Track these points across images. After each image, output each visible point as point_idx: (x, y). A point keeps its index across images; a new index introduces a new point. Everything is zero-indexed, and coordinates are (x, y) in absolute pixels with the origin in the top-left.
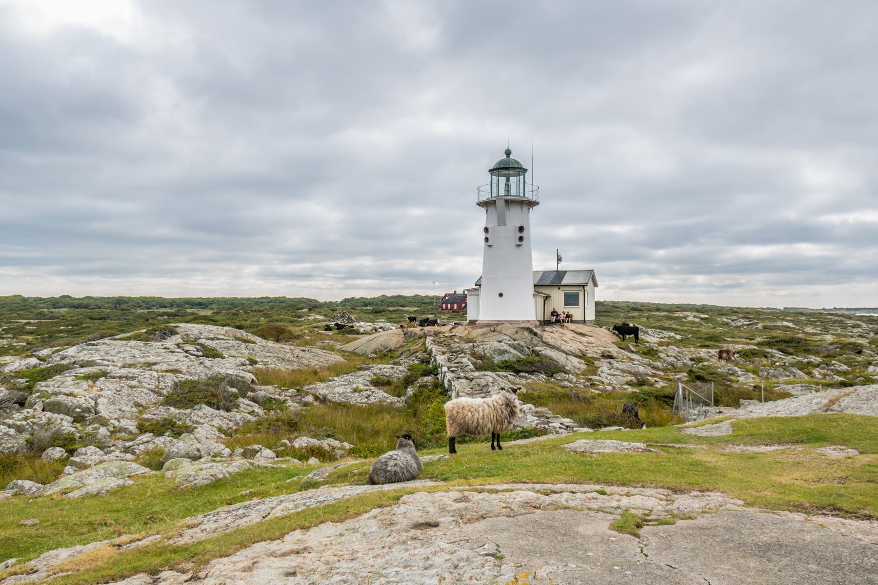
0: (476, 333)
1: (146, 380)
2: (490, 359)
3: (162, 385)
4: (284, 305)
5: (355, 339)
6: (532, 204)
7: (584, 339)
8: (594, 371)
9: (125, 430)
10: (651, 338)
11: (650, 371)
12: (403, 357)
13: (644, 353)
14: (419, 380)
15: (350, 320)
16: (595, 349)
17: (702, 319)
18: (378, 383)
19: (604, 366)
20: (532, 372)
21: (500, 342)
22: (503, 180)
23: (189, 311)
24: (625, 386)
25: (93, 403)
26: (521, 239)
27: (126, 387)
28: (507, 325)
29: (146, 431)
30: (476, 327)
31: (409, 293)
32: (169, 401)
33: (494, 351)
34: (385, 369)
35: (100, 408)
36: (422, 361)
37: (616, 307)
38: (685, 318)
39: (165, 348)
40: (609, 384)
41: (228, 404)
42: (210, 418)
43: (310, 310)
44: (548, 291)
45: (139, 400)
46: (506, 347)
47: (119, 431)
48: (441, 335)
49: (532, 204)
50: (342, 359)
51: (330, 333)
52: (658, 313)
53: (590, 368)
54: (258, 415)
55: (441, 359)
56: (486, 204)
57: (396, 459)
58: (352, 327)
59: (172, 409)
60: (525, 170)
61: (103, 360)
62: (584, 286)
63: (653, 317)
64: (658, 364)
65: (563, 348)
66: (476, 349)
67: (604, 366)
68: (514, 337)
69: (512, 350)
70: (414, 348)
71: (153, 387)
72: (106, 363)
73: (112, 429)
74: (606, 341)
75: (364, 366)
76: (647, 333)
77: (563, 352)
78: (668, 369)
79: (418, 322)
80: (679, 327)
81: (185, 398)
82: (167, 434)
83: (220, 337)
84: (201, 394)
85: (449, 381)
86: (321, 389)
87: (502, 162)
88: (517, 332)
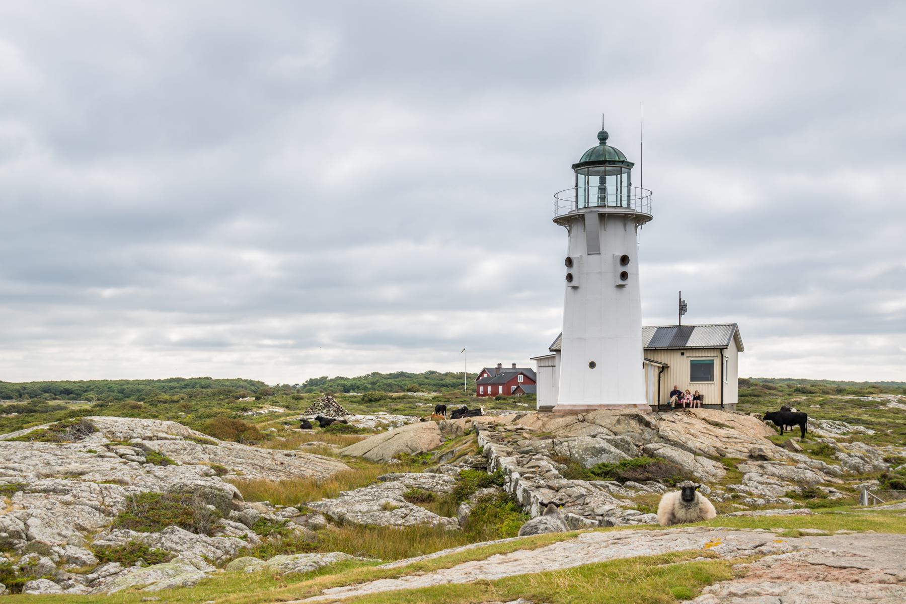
1: (84, 494)
2: (580, 463)
3: (108, 501)
4: (209, 391)
5: (358, 440)
6: (641, 219)
7: (722, 432)
8: (739, 478)
9: (75, 560)
10: (826, 432)
11: (822, 477)
12: (442, 463)
13: (814, 453)
14: (477, 493)
15: (339, 411)
16: (739, 446)
18: (416, 497)
19: (752, 470)
20: (644, 481)
21: (594, 436)
23: (52, 403)
24: (784, 499)
25: (22, 525)
26: (624, 276)
27: (58, 504)
28: (604, 411)
29: (109, 560)
30: (554, 416)
32: (124, 522)
33: (586, 450)
34: (423, 479)
35: (33, 531)
36: (476, 467)
37: (770, 388)
38: (883, 403)
39: (90, 451)
40: (761, 496)
41: (209, 526)
43: (257, 399)
44: (665, 358)
47: (68, 562)
48: (501, 429)
49: (641, 219)
52: (839, 397)
53: (732, 474)
54: (252, 541)
55: (506, 462)
56: (567, 221)
58: (345, 422)
59: (133, 533)
60: (630, 165)
61: (6, 468)
62: (721, 349)
63: (831, 402)
64: (836, 467)
65: (690, 444)
66: (557, 448)
67: (752, 470)
68: (615, 429)
69: (613, 449)
70: (459, 448)
71: (97, 503)
72: (11, 472)
73: (58, 559)
74: (755, 435)
75: (387, 475)
76: (819, 426)
77: (690, 450)
78: (850, 475)
79: (449, 414)
81: (147, 518)
82: (139, 563)
83: (161, 435)
84: (168, 512)
85: (525, 491)
86: (336, 507)
87: (593, 151)
88: (619, 422)
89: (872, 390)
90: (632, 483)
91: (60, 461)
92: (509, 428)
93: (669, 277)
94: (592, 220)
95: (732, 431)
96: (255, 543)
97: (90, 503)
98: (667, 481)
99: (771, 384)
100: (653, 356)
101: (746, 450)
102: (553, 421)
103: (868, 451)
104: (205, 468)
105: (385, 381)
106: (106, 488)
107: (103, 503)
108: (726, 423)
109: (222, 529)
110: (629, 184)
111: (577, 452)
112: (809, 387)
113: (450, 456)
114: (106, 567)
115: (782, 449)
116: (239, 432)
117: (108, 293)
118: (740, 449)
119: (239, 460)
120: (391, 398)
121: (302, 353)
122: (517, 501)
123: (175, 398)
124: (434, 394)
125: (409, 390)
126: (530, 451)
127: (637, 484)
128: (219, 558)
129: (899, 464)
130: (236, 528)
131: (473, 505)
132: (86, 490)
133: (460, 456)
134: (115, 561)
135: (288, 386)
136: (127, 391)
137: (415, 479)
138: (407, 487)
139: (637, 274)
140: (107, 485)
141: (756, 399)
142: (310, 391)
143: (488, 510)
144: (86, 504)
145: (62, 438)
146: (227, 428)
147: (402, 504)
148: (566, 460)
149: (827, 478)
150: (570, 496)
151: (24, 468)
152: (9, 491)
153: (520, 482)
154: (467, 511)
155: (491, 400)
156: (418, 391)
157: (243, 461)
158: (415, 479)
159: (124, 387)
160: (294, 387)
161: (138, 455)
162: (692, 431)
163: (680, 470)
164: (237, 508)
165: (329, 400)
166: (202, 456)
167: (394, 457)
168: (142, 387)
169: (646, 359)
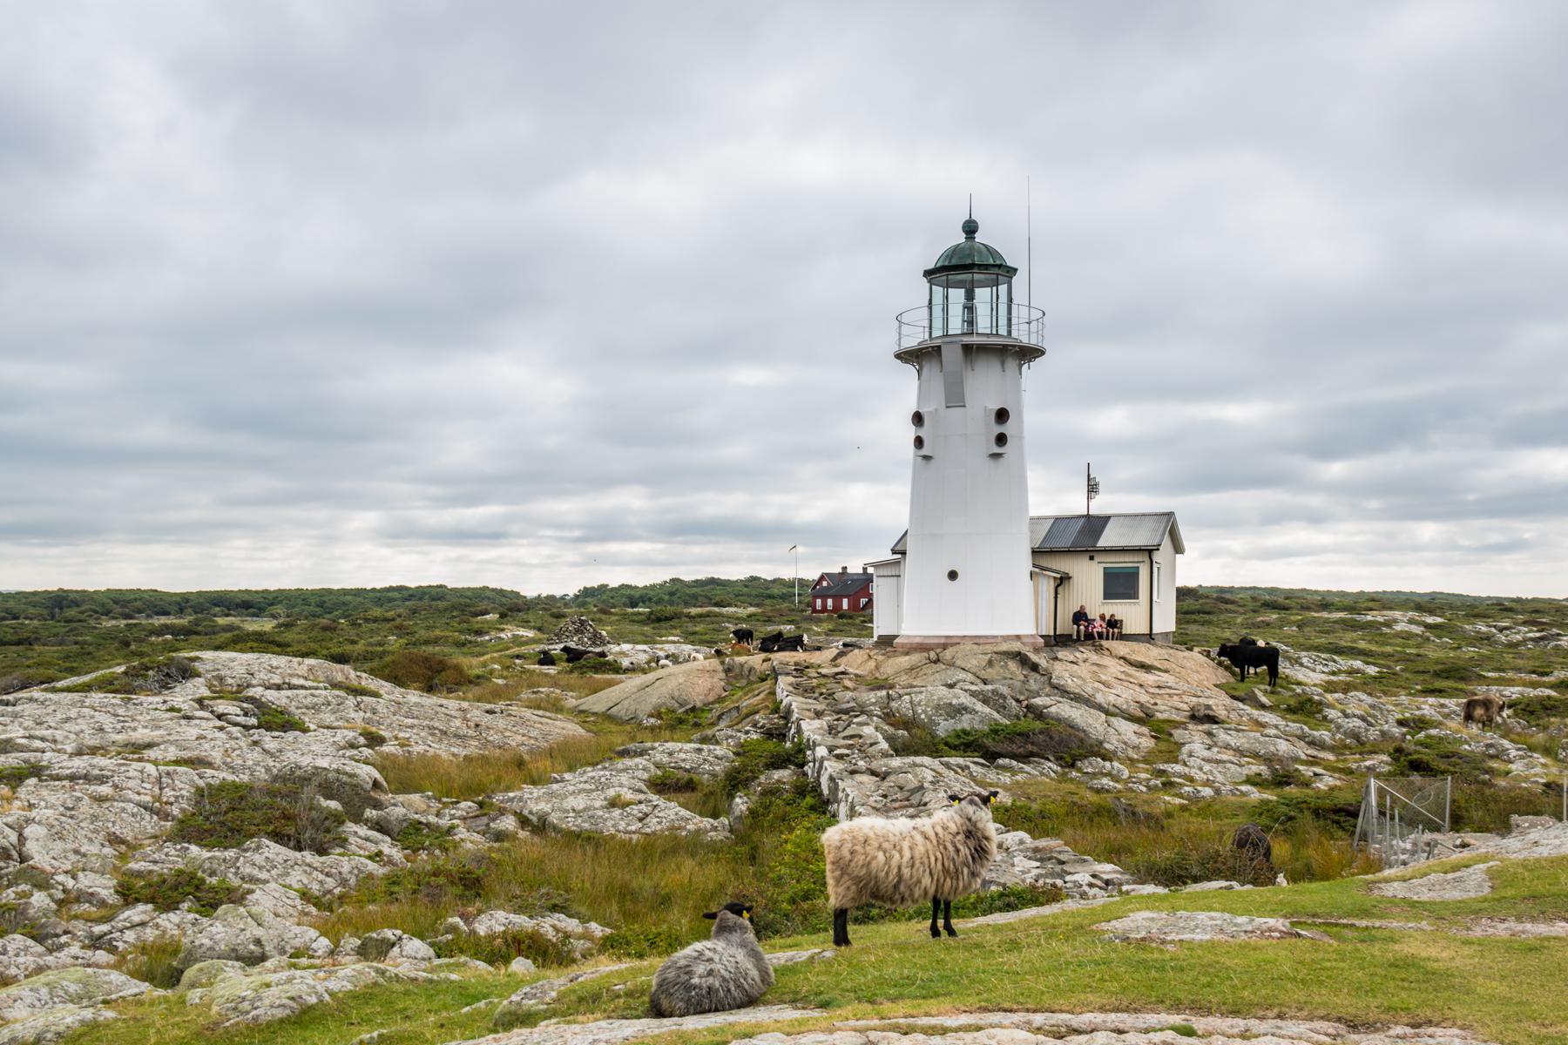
0: (894, 665)
1: (131, 784)
5: (610, 684)
6: (1029, 353)
8: (1173, 753)
9: (90, 897)
11: (1303, 751)
12: (722, 724)
14: (762, 778)
15: (596, 639)
16: (1176, 702)
17: (1428, 626)
18: (667, 785)
19: (1195, 741)
20: (1024, 758)
21: (951, 686)
22: (957, 295)
23: (221, 621)
24: (1244, 788)
25: (14, 838)
26: (1001, 439)
28: (968, 646)
29: (137, 900)
30: (895, 653)
31: (735, 572)
32: (186, 832)
33: (938, 707)
34: (682, 752)
35: (31, 847)
36: (769, 734)
37: (1227, 602)
38: (1388, 624)
39: (172, 709)
40: (1207, 783)
42: (280, 870)
43: (503, 616)
45: (117, 830)
46: (965, 699)
47: (78, 900)
49: (1029, 353)
51: (551, 670)
52: (1325, 615)
53: (1163, 746)
54: (390, 862)
55: (812, 729)
57: (710, 960)
58: (603, 655)
59: (194, 849)
61: (30, 737)
62: (1149, 551)
63: (1314, 622)
64: (1324, 735)
65: (1100, 698)
66: (894, 705)
67: (1195, 741)
68: (983, 674)
69: (979, 707)
70: (747, 702)
71: (148, 798)
72: (38, 744)
73: (60, 896)
74: (1200, 683)
75: (632, 746)
76: (1298, 662)
77: (1100, 708)
79: (757, 643)
80: (1374, 648)
81: (223, 824)
82: (185, 905)
83: (295, 681)
84: (258, 815)
85: (832, 779)
86: (535, 800)
87: (955, 250)
88: (990, 663)
89: (1371, 604)
91: (119, 726)
92: (824, 671)
93: (1081, 444)
95: (1166, 678)
96: (395, 865)
97: (137, 798)
98: (1062, 758)
99: (1228, 596)
100: (1046, 562)
101: (1185, 707)
102: (891, 661)
103: (1372, 707)
104: (350, 735)
105: (688, 591)
106: (168, 774)
107: (158, 799)
108: (1156, 664)
109: (343, 842)
110: (1010, 300)
111: (924, 712)
112: (1281, 600)
113: (735, 714)
114: (127, 913)
115: (1241, 705)
116: (432, 675)
118: (1177, 704)
119: (409, 721)
120: (688, 616)
121: (593, 548)
122: (821, 794)
123: (390, 614)
124: (752, 610)
126: (852, 709)
128: (330, 892)
129: (1421, 729)
130: (367, 839)
131: (754, 798)
132: (137, 778)
133: (747, 716)
134: (147, 902)
135: (552, 597)
136: (328, 604)
137: (670, 754)
138: (658, 766)
139: (1021, 438)
140: (171, 768)
141: (1207, 617)
142: (583, 604)
143: (773, 809)
144: (130, 801)
145: (141, 687)
146: (415, 668)
147: (641, 797)
148: (908, 724)
149: (1310, 752)
150: (901, 788)
151: (59, 738)
152: (15, 778)
153: (826, 763)
154: (744, 808)
155: (830, 619)
156: (729, 605)
157: (416, 722)
158: (670, 754)
160: (562, 598)
161: (246, 714)
162: (1104, 678)
163: (1082, 741)
164: (378, 805)
165: (582, 623)
166: (353, 715)
167: (651, 716)
168: (349, 598)
169: (1035, 566)
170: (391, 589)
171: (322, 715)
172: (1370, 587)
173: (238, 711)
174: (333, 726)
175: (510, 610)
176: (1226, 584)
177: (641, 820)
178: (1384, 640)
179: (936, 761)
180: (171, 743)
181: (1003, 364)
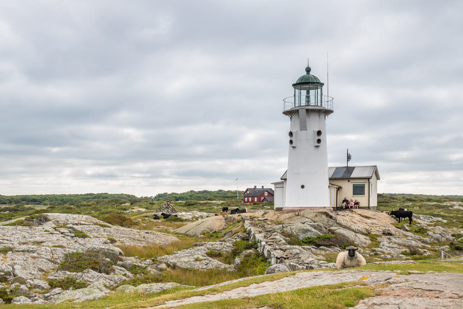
0: (284, 217)
1: (43, 253)
2: (297, 237)
3: (55, 256)
4: (107, 200)
5: (183, 225)
6: (328, 112)
8: (378, 245)
9: (39, 287)
10: (422, 221)
11: (420, 244)
12: (226, 237)
13: (416, 232)
14: (244, 252)
15: (173, 210)
16: (378, 229)
18: (213, 254)
19: (384, 241)
21: (303, 223)
23: (26, 206)
24: (401, 255)
25: (11, 269)
26: (319, 141)
27: (30, 258)
28: (309, 210)
29: (56, 287)
31: (213, 188)
32: (63, 267)
33: (300, 230)
34: (216, 245)
35: (17, 272)
36: (243, 239)
37: (394, 199)
38: (451, 206)
39: (46, 231)
40: (389, 254)
41: (107, 269)
42: (96, 279)
43: (132, 204)
44: (340, 183)
45: (41, 267)
48: (256, 219)
49: (328, 112)
50: (177, 239)
51: (159, 221)
52: (429, 203)
53: (374, 243)
54: (129, 277)
55: (259, 236)
56: (289, 113)
57: (279, 268)
58: (176, 216)
59: (68, 272)
61: (3, 239)
62: (368, 179)
63: (425, 206)
64: (427, 239)
65: (353, 227)
66: (285, 229)
67: (384, 241)
68: (314, 219)
69: (313, 230)
70: (234, 229)
71: (50, 257)
72: (6, 241)
73: (30, 286)
75: (198, 243)
76: (419, 218)
77: (353, 230)
78: (434, 243)
79: (229, 212)
80: (446, 215)
81: (75, 265)
82: (71, 288)
83: (82, 222)
84: (86, 262)
85: (268, 251)
86: (172, 259)
87: (303, 77)
88: (316, 216)
89: (445, 200)
90: (323, 247)
92: (260, 219)
93: (342, 141)
94: (302, 113)
95: (374, 221)
96: (130, 278)
97: (46, 257)
98: (341, 246)
99: (394, 197)
100: (333, 182)
103: (444, 231)
104: (105, 239)
105: (197, 195)
107: (53, 257)
108: (371, 216)
109: (113, 271)
110: (322, 94)
111: (295, 231)
112: (413, 198)
114: (54, 290)
115: (399, 230)
117: (55, 150)
120: (200, 204)
121: (155, 180)
122: (264, 256)
123: (90, 203)
124: (222, 202)
125: (209, 200)
126: (271, 231)
127: (325, 248)
128: (112, 285)
129: (460, 237)
130: (121, 270)
135: (147, 197)
137: (212, 245)
139: (325, 140)
140: (55, 248)
141: (386, 204)
143: (249, 261)
146: (116, 219)
147: (205, 258)
148: (289, 236)
149: (422, 245)
150: (291, 254)
151: (12, 240)
152: (5, 251)
153: (266, 247)
154: (239, 261)
155: (251, 204)
157: (124, 236)
158: (212, 245)
159: (63, 198)
160: (150, 198)
161: (70, 233)
162: (354, 221)
163: (347, 241)
166: (103, 233)
168: (72, 198)
169: (330, 184)
170: (88, 194)
171: (93, 233)
172: (446, 194)
173: (68, 232)
174: (98, 237)
175: (134, 201)
176: (393, 193)
177: (206, 265)
178: (450, 212)
179: (300, 247)
180: (49, 241)
181: (319, 116)
